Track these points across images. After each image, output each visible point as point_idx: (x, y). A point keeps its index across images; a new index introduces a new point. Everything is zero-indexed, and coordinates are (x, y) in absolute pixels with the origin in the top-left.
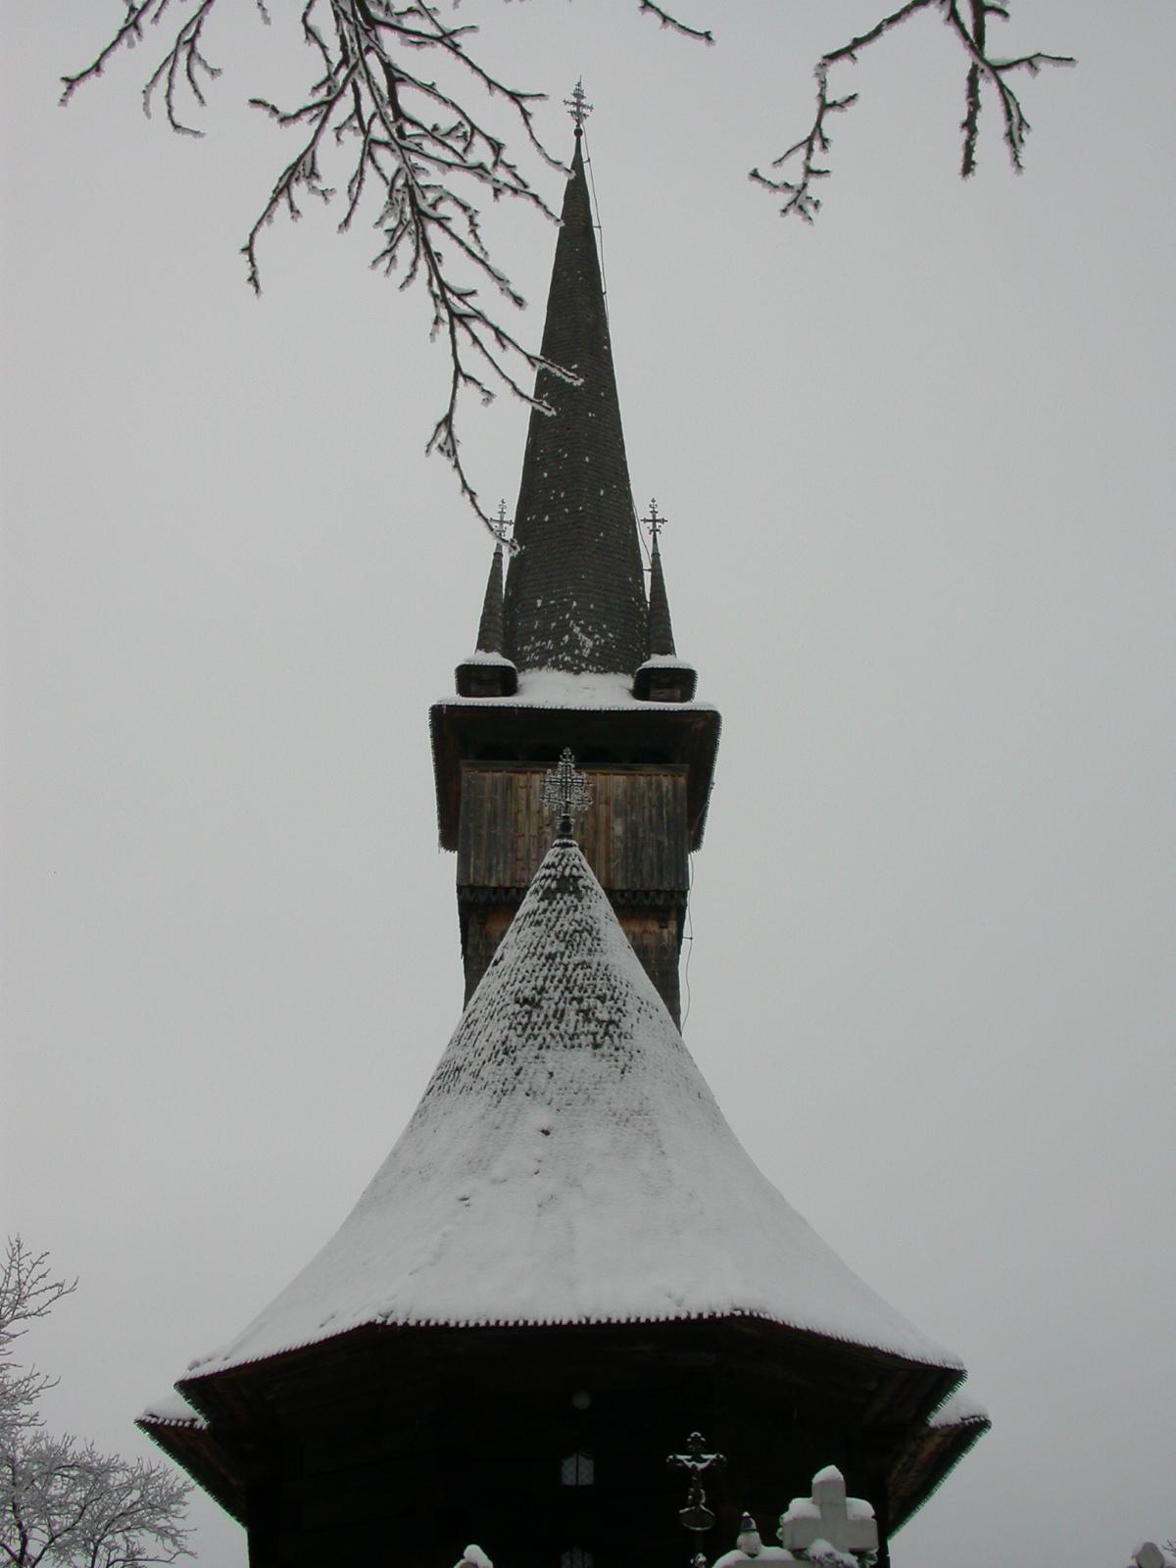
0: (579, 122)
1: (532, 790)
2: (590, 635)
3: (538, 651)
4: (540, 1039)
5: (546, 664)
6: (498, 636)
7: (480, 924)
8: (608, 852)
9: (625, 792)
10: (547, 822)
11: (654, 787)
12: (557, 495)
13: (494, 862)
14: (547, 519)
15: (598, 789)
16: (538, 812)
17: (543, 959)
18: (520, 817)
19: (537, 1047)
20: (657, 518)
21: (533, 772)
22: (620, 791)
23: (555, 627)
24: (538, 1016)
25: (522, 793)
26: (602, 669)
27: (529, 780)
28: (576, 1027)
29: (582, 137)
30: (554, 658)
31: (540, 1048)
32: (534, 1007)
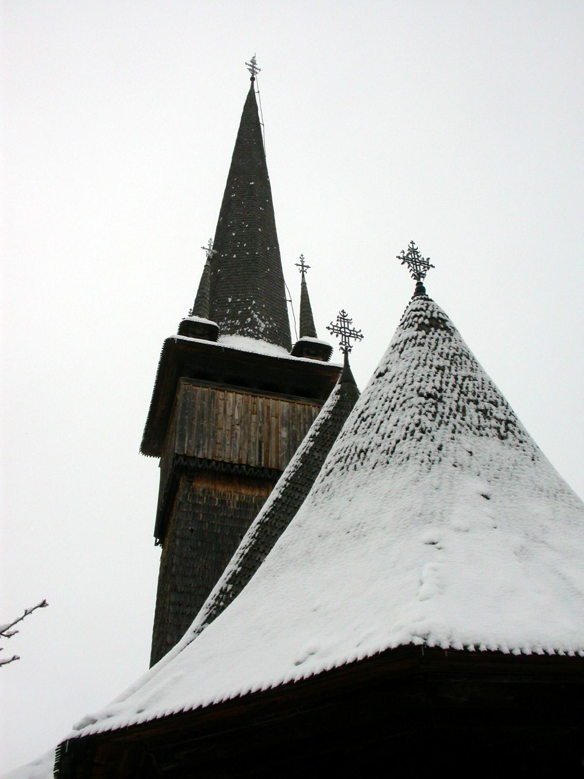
0: (253, 74)
1: (228, 402)
2: (263, 321)
3: (229, 325)
4: (450, 426)
5: (235, 333)
6: (206, 310)
7: (188, 481)
8: (277, 447)
9: (288, 412)
10: (237, 423)
11: (307, 412)
12: (241, 245)
13: (201, 442)
14: (235, 256)
15: (271, 408)
16: (232, 416)
17: (434, 369)
18: (220, 417)
19: (450, 430)
20: (304, 265)
21: (229, 391)
22: (285, 411)
23: (241, 313)
24: (444, 408)
25: (221, 403)
26: (271, 341)
27: (225, 395)
28: (479, 421)
29: (255, 82)
30: (241, 330)
31: (453, 432)
32: (438, 401)
